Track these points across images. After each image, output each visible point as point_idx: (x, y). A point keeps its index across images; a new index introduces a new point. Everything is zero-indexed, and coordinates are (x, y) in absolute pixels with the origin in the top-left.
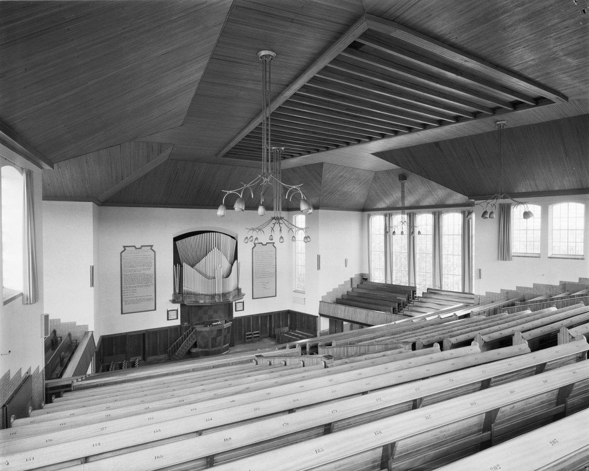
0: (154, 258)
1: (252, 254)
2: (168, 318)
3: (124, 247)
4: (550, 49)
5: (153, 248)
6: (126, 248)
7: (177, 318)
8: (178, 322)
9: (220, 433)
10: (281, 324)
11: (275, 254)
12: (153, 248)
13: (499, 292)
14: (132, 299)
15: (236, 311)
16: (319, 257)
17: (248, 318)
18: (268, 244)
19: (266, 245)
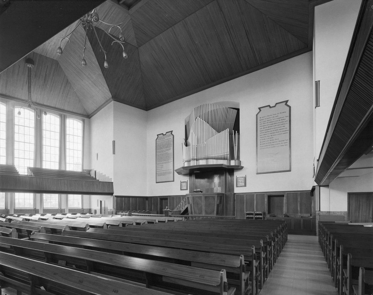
0: (172, 140)
1: (257, 125)
2: (181, 188)
3: (259, 108)
4: (99, 91)
5: (288, 104)
6: (261, 109)
7: (187, 189)
8: (186, 192)
9: (33, 163)
10: (299, 209)
11: (288, 115)
12: (288, 104)
13: (242, 165)
14: (161, 172)
15: (237, 186)
16: (114, 153)
17: (251, 195)
18: (277, 105)
19: (274, 106)
